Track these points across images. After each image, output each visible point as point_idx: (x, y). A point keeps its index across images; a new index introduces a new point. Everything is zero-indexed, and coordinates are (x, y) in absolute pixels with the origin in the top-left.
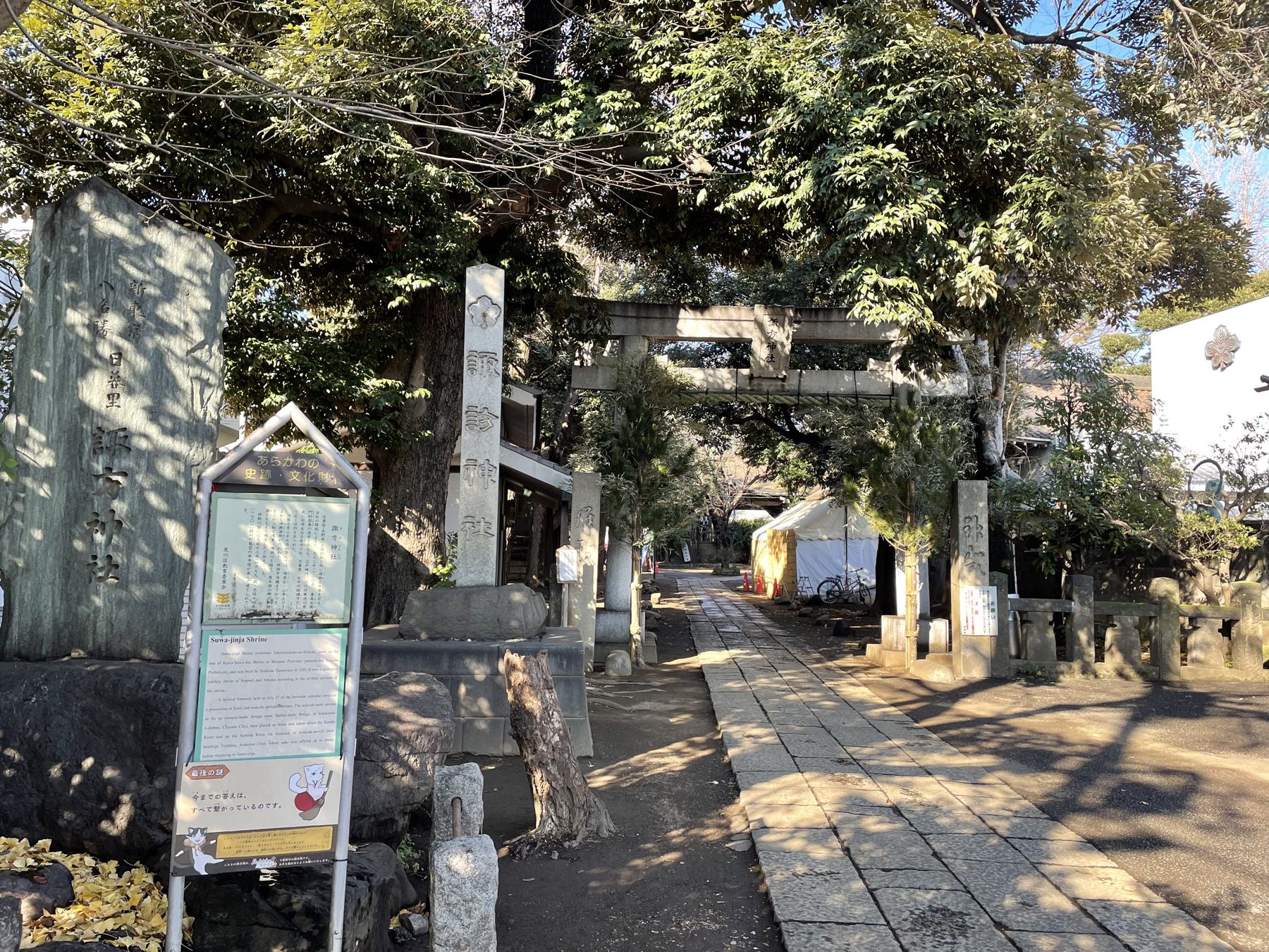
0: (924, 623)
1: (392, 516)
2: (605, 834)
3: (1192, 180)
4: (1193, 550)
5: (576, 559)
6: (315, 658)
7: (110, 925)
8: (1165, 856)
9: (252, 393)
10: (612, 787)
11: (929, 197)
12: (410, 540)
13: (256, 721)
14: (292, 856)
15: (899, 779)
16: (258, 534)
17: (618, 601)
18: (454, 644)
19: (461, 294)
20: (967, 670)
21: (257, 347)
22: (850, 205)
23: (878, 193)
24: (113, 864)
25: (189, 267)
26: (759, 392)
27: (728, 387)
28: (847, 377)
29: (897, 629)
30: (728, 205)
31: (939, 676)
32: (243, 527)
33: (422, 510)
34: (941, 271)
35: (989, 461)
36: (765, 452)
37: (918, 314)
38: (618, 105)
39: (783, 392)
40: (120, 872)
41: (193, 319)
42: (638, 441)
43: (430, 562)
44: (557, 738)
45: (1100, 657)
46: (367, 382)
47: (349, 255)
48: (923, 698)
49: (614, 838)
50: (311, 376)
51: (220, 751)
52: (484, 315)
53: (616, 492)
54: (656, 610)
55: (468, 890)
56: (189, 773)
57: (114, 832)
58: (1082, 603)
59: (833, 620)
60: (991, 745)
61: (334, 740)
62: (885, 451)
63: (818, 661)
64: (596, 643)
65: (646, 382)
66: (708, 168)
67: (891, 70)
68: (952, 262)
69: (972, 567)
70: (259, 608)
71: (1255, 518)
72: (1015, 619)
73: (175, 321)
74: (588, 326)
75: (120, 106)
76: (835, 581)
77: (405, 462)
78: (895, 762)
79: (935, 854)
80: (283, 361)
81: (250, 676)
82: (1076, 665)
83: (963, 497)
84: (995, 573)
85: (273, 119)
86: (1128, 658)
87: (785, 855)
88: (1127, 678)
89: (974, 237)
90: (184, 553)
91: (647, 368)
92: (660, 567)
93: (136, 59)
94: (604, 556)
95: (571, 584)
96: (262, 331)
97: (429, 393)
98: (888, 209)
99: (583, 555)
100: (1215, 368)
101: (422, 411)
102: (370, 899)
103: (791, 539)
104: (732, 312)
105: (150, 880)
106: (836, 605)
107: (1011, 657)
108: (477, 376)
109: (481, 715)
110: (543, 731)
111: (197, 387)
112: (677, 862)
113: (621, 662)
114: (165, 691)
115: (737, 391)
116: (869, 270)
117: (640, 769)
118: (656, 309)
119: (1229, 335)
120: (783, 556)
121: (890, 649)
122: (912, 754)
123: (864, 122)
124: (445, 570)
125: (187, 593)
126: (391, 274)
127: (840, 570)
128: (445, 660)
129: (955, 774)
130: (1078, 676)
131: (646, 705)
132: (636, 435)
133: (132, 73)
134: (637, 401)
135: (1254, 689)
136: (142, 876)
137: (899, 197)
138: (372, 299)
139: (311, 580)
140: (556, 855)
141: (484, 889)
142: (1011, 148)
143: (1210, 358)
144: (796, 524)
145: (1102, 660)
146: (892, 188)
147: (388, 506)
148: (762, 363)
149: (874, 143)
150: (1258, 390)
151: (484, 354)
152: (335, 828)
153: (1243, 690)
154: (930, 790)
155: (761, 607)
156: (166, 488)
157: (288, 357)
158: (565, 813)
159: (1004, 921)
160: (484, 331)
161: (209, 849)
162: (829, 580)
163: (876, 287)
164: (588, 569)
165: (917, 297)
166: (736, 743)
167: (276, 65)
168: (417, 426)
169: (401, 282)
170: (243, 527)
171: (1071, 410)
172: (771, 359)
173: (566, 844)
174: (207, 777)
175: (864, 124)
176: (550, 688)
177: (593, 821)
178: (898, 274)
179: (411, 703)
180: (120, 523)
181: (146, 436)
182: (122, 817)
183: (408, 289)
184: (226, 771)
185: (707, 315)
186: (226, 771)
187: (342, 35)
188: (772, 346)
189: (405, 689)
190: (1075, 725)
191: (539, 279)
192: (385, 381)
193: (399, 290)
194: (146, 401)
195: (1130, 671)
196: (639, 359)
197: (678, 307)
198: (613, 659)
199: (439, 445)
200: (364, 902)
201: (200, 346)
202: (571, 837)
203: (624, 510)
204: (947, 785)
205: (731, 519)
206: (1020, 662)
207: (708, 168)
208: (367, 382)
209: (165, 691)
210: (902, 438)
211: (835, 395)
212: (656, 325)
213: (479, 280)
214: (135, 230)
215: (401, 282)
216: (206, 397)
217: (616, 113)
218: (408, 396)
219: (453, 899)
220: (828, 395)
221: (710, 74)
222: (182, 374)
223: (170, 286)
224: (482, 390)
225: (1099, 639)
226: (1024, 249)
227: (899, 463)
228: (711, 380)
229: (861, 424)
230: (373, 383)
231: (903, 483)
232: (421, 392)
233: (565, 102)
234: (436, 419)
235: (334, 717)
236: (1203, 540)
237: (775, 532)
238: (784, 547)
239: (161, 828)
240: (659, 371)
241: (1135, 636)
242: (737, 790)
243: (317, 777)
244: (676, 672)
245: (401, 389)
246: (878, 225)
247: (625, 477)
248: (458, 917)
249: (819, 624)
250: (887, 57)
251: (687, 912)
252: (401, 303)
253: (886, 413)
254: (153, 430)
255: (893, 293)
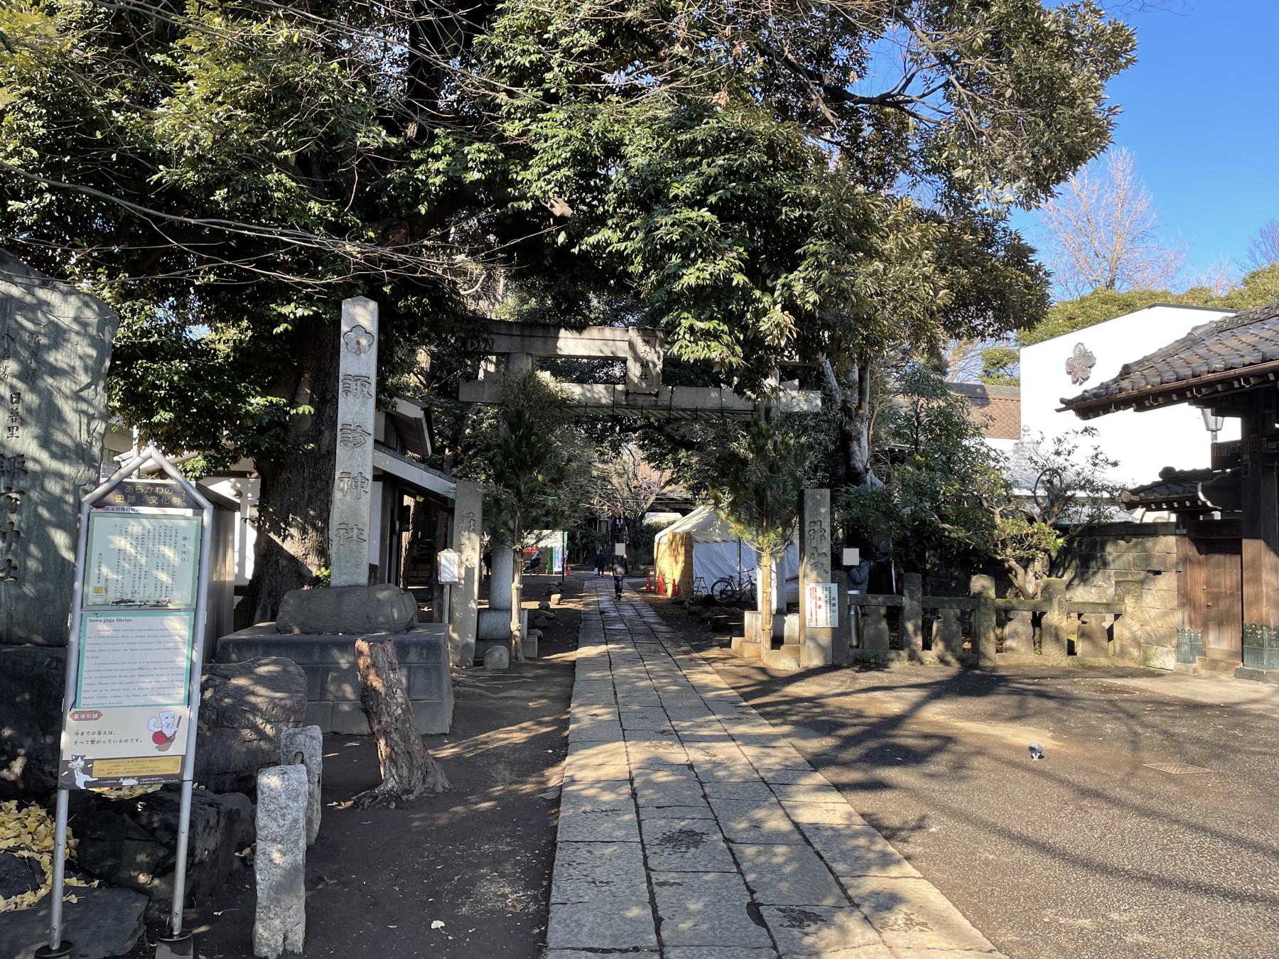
0: (779, 617)
1: (278, 523)
2: (440, 789)
3: (1003, 225)
4: (1009, 551)
5: (459, 561)
6: (167, 634)
7: (11, 843)
8: (887, 795)
9: (143, 410)
10: (457, 757)
11: (734, 254)
12: (293, 545)
13: (123, 680)
14: (151, 777)
15: (703, 744)
16: (122, 543)
17: (500, 601)
18: (327, 637)
19: (337, 324)
20: (810, 659)
21: (147, 369)
22: (670, 259)
23: (689, 249)
24: (13, 804)
25: (76, 319)
26: (634, 407)
27: (604, 401)
28: (714, 394)
29: (756, 622)
30: (583, 247)
31: (783, 663)
32: (110, 537)
33: (306, 517)
34: (749, 315)
35: (855, 469)
36: (669, 457)
37: (726, 352)
38: (483, 156)
39: (656, 406)
40: (19, 809)
41: (78, 364)
42: (519, 451)
43: (314, 567)
44: (400, 711)
45: (927, 646)
46: (253, 401)
47: (239, 280)
48: (760, 683)
49: (446, 793)
50: (198, 395)
51: (93, 701)
52: (358, 343)
53: (497, 501)
54: (553, 610)
55: (283, 800)
56: (72, 716)
57: (12, 777)
58: (912, 598)
59: (710, 615)
60: (794, 718)
61: (182, 693)
62: (744, 462)
63: (685, 653)
64: (478, 639)
65: (528, 397)
66: (568, 212)
67: (705, 146)
68: (757, 309)
69: (815, 566)
70: (125, 598)
71: (1066, 522)
72: (856, 613)
73: (65, 367)
74: (472, 344)
75: (19, 154)
76: (728, 581)
77: (292, 475)
78: (705, 732)
79: (705, 796)
80: (171, 382)
81: (118, 647)
82: (904, 654)
83: (809, 504)
84: (837, 572)
85: (161, 167)
86: (948, 646)
87: (578, 799)
88: (947, 664)
89: (778, 287)
90: (69, 556)
91: (530, 386)
92: (572, 569)
93: (34, 109)
94: (488, 559)
95: (452, 585)
96: (151, 353)
97: (312, 410)
98: (699, 264)
99: (464, 558)
100: (1074, 382)
101: (307, 426)
102: (218, 822)
103: (688, 541)
104: (608, 333)
105: (44, 814)
106: (727, 605)
107: (851, 647)
108: (351, 398)
109: (346, 699)
110: (388, 705)
111: (85, 420)
112: (494, 808)
113: (500, 656)
114: (56, 668)
115: (616, 404)
116: (685, 315)
117: (485, 743)
118: (536, 327)
119: (1086, 352)
120: (681, 559)
121: (750, 642)
122: (726, 726)
123: (683, 188)
124: (326, 573)
125: (316, 827)
126: (274, 301)
127: (733, 570)
128: (317, 651)
129: (748, 740)
130: (906, 663)
131: (514, 693)
132: (518, 447)
133: (31, 124)
134: (520, 414)
135: (1046, 673)
136: (37, 811)
137: (709, 254)
138: (264, 323)
139: (163, 577)
140: (393, 805)
141: (296, 800)
142: (801, 216)
143: (1069, 373)
144: (694, 527)
145: (930, 649)
146: (701, 246)
147: (274, 513)
148: (636, 380)
149: (691, 207)
150: (1059, 411)
151: (357, 378)
152: (184, 757)
153: (1031, 674)
154: (725, 751)
155: (655, 606)
156: (54, 503)
157: (176, 378)
158: (405, 772)
159: (733, 837)
160: (358, 360)
161: (87, 771)
162: (722, 580)
163: (691, 329)
164: (469, 571)
165: (726, 338)
166: (577, 720)
167: (166, 119)
168: (302, 439)
169: (286, 310)
170: (110, 537)
171: (919, 423)
172: (645, 375)
173: (404, 797)
174: (86, 719)
175: (682, 188)
176: (393, 670)
177: (429, 780)
178: (711, 318)
179: (269, 682)
180: (18, 533)
181: (36, 460)
182: (18, 766)
183: (292, 316)
184: (100, 715)
185: (586, 334)
186: (100, 715)
187: (225, 96)
188: (645, 365)
189: (262, 670)
190: (883, 702)
191: (419, 304)
192: (269, 398)
193: (284, 318)
194: (36, 431)
195: (949, 658)
196: (520, 376)
197: (558, 327)
198: (491, 654)
199: (323, 456)
200: (213, 822)
201: (88, 386)
202: (409, 792)
203: (505, 515)
204: (743, 748)
205: (645, 522)
206: (858, 651)
207: (568, 212)
208: (253, 401)
209: (56, 668)
210: (759, 450)
211: (703, 410)
212: (539, 343)
213: (351, 310)
214: (29, 289)
215: (286, 310)
216: (92, 427)
217: (482, 163)
218: (293, 412)
219: (272, 807)
220: (696, 410)
221: (562, 134)
222: (67, 408)
223: (58, 335)
224: (357, 410)
225: (926, 630)
226: (811, 300)
227: (756, 473)
228: (588, 394)
229: (725, 437)
230: (258, 401)
231: (759, 492)
232: (306, 409)
233: (438, 149)
234: (321, 432)
235: (183, 677)
236: (1020, 541)
237: (674, 535)
238: (682, 550)
239: (51, 774)
240: (540, 387)
241: (955, 627)
242: (566, 755)
243: (170, 720)
244: (553, 666)
245: (285, 405)
246: (690, 278)
247: (505, 486)
248: (275, 820)
249: (703, 621)
250: (700, 132)
251: (489, 840)
252: (286, 329)
253: (747, 426)
254: (44, 456)
255: (707, 334)
